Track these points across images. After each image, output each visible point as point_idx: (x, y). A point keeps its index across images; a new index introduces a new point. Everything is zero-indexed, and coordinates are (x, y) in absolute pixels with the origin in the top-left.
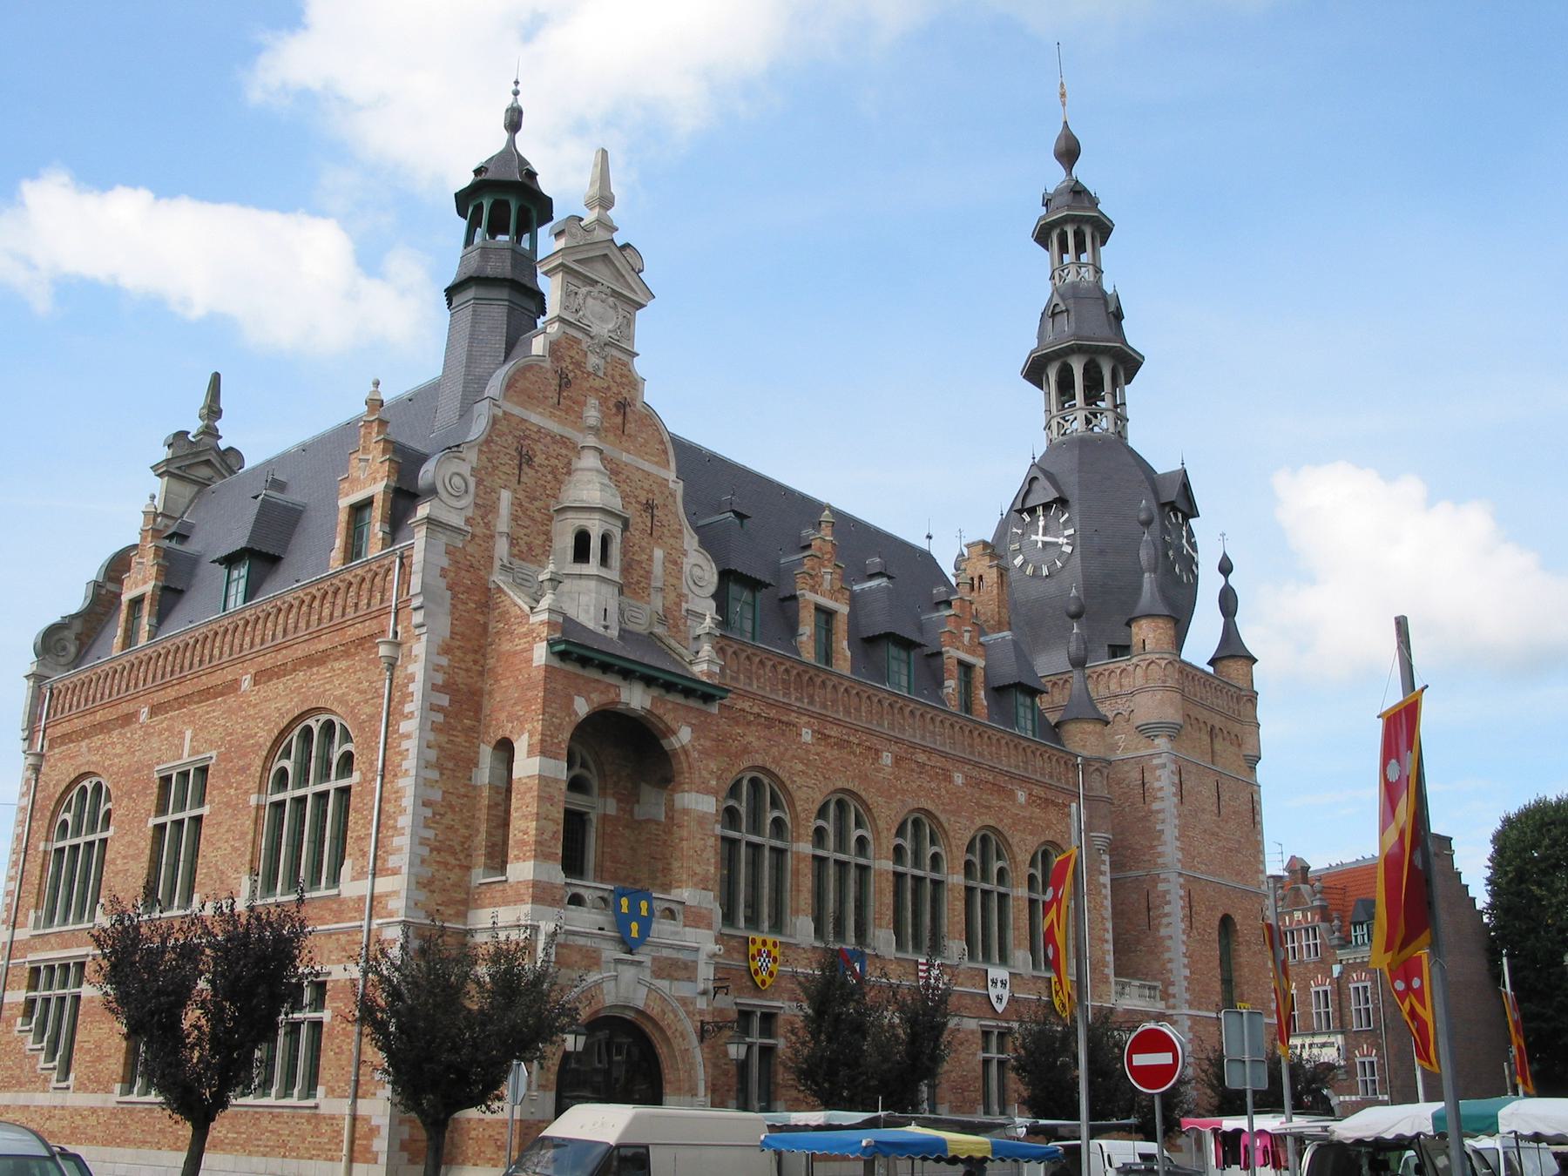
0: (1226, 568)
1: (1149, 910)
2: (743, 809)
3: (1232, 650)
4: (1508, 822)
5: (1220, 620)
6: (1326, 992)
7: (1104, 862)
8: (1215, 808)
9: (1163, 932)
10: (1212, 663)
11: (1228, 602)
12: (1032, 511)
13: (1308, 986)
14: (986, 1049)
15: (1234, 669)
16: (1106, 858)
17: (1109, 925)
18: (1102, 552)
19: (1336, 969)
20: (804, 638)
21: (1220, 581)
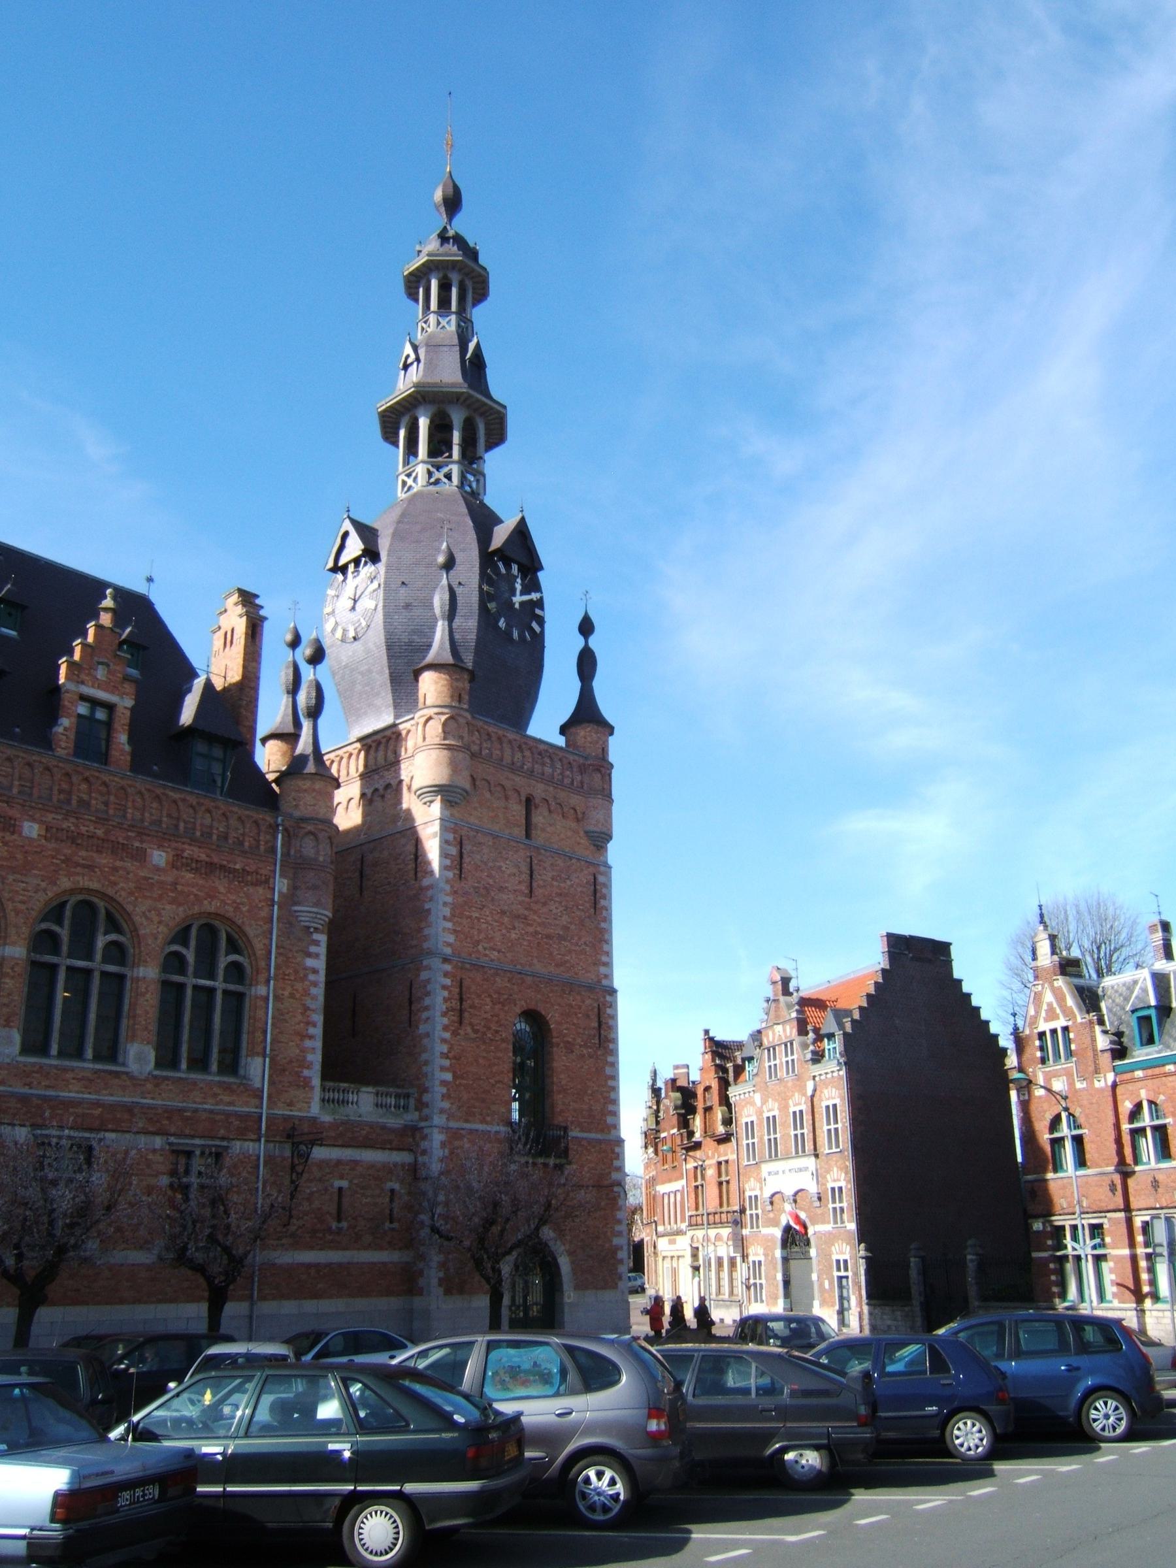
0: (586, 627)
1: (411, 1003)
2: (190, 956)
3: (587, 715)
4: (612, 766)
5: (576, 685)
6: (801, 1112)
7: (317, 943)
8: (524, 888)
9: (423, 1028)
10: (564, 730)
11: (586, 664)
12: (343, 569)
13: (787, 1107)
14: (696, 1180)
15: (584, 733)
16: (323, 938)
17: (319, 1018)
18: (407, 606)
19: (810, 1085)
20: (60, 730)
21: (579, 643)
